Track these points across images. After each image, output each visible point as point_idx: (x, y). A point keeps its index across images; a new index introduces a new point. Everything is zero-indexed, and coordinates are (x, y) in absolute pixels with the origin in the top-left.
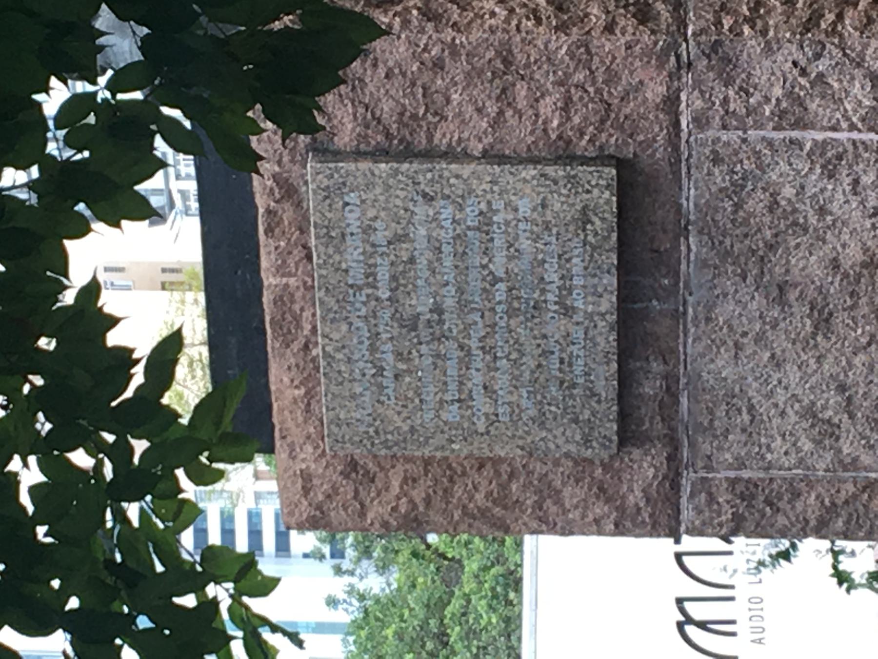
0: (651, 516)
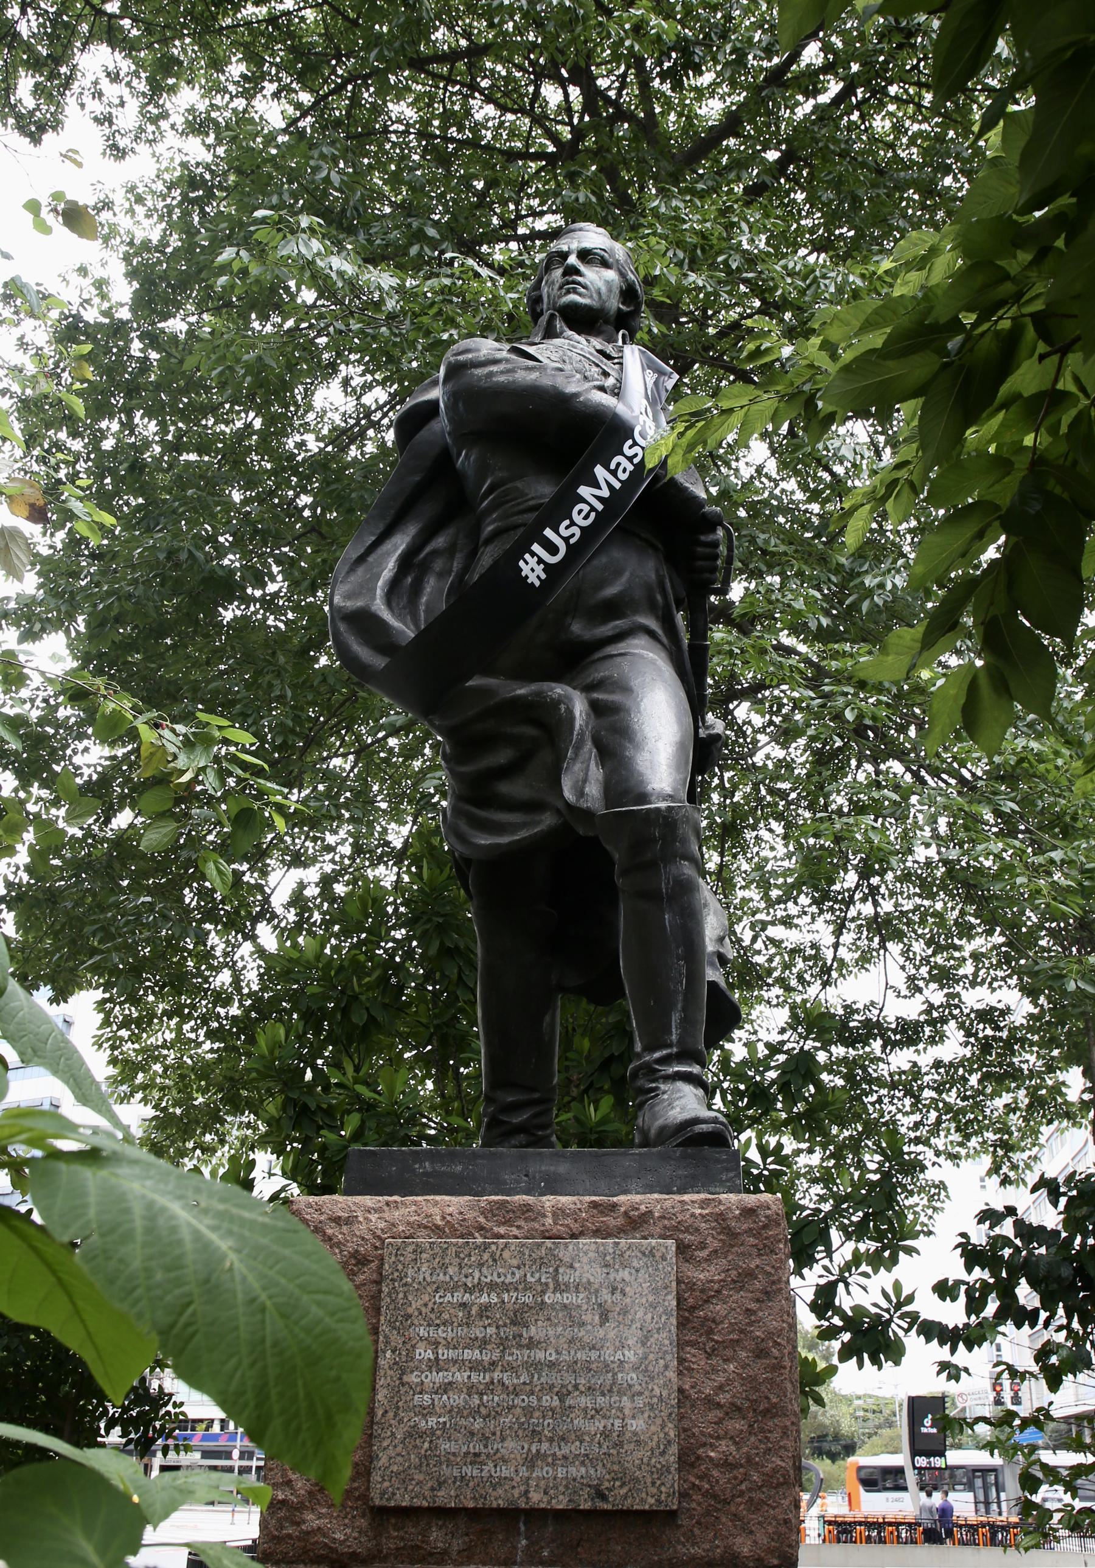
0: (289, 1536)
